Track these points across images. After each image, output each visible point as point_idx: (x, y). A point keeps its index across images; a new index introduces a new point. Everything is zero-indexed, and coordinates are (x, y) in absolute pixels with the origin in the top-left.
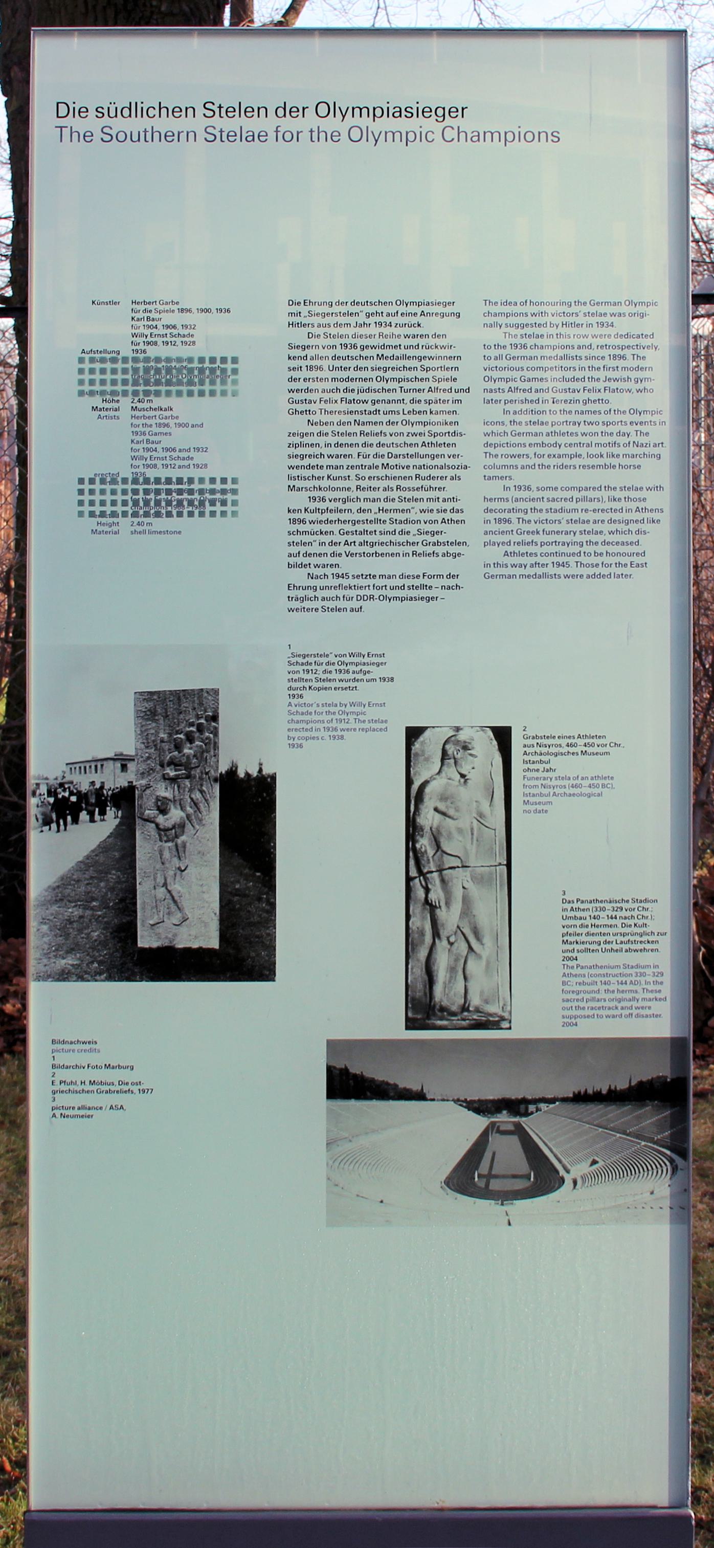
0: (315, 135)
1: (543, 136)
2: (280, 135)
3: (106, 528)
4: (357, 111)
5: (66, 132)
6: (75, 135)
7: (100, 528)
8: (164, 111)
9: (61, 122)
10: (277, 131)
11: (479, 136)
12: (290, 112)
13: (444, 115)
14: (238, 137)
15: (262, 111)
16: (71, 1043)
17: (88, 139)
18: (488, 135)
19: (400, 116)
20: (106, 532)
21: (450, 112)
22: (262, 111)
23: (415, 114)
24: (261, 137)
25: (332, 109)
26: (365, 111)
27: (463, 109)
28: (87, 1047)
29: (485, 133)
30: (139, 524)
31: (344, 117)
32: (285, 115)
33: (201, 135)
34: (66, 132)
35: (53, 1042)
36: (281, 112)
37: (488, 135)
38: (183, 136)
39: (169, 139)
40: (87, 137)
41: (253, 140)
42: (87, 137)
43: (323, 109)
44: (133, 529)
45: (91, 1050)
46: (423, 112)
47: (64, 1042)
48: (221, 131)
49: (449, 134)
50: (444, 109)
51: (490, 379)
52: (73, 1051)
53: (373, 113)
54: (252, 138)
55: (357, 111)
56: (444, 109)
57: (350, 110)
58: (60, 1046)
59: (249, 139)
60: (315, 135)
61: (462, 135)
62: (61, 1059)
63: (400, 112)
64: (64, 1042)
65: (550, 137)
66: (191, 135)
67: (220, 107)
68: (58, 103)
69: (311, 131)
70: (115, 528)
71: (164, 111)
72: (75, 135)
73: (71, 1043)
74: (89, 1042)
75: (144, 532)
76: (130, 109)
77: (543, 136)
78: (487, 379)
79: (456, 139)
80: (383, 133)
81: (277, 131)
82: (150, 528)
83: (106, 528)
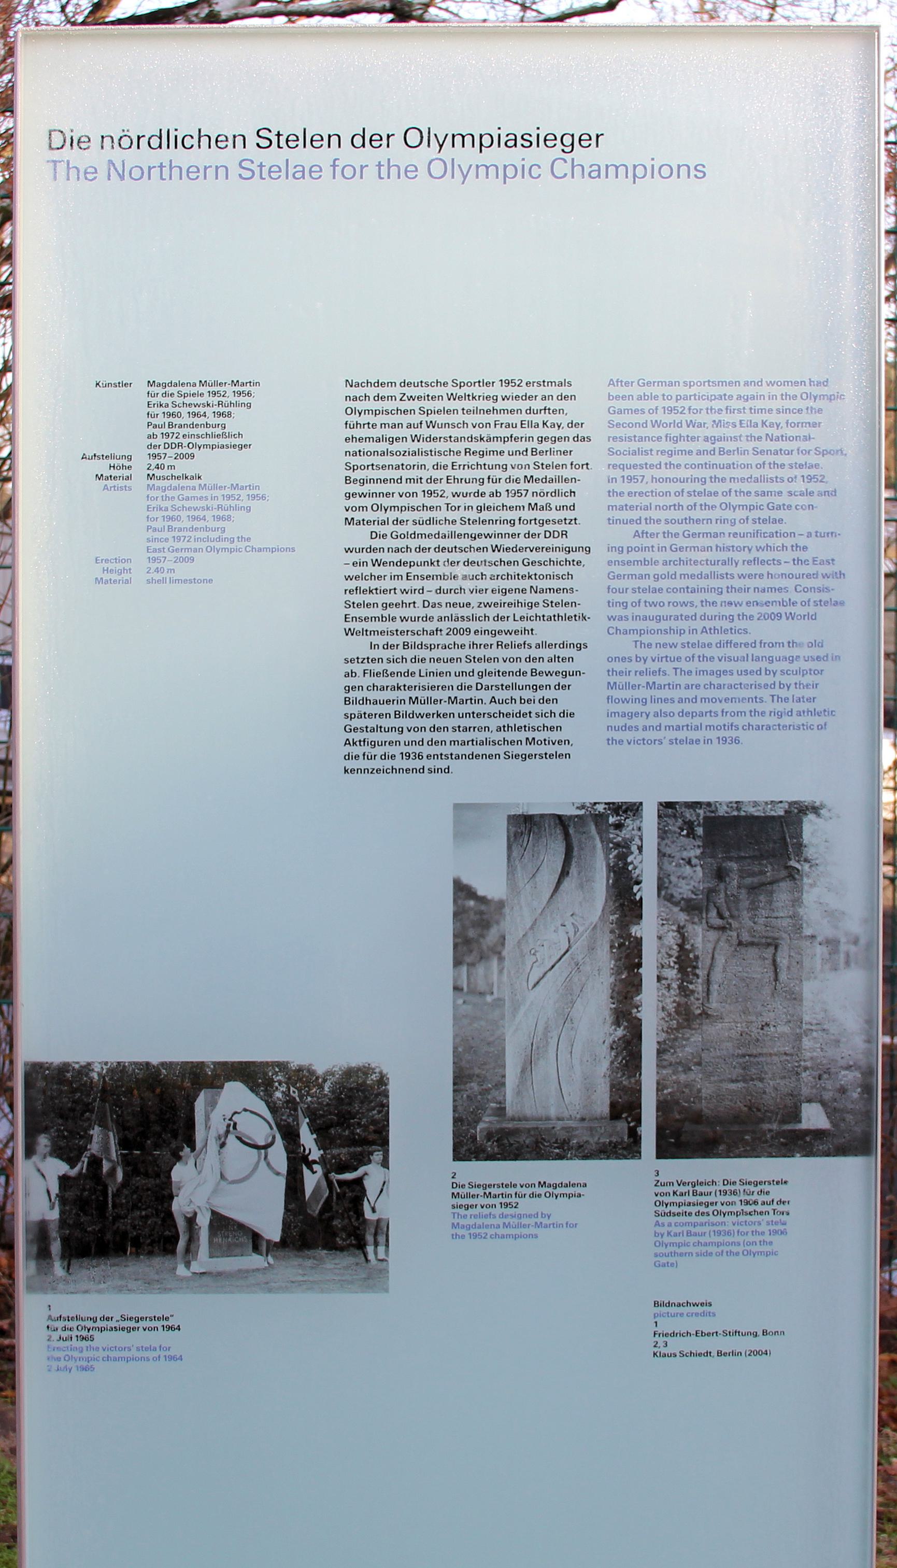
0: (384, 170)
1: (684, 170)
2: (338, 170)
3: (114, 576)
4: (458, 139)
5: (62, 168)
6: (73, 173)
7: (106, 576)
8: (205, 140)
9: (56, 155)
10: (334, 166)
11: (599, 171)
12: (371, 140)
13: (572, 144)
14: (283, 173)
15: (334, 140)
16: (679, 1305)
17: (90, 177)
18: (612, 170)
19: (515, 145)
20: (115, 581)
21: (580, 140)
22: (334, 140)
23: (535, 143)
24: (313, 172)
25: (425, 137)
26: (468, 139)
27: (598, 136)
28: (700, 1309)
29: (607, 167)
30: (157, 570)
31: (441, 146)
32: (363, 145)
33: (234, 171)
34: (62, 168)
35: (656, 1304)
36: (358, 141)
37: (612, 170)
38: (211, 172)
39: (192, 176)
40: (89, 174)
41: (303, 177)
42: (89, 174)
43: (413, 138)
44: (149, 576)
45: (704, 1314)
46: (545, 140)
47: (669, 1304)
48: (261, 166)
49: (560, 168)
50: (180, 168)
51: (353, 411)
52: (681, 1315)
53: (480, 143)
54: (302, 173)
55: (458, 139)
56: (573, 136)
57: (449, 138)
58: (664, 1310)
59: (297, 175)
60: (384, 170)
61: (578, 170)
62: (666, 1325)
63: (515, 140)
64: (669, 1304)
65: (693, 172)
66: (222, 171)
67: (279, 135)
68: (50, 132)
69: (379, 165)
70: (126, 576)
71: (205, 140)
72: (73, 173)
73: (679, 1305)
74: (702, 1304)
75: (163, 581)
76: (160, 138)
77: (684, 170)
78: (349, 411)
79: (569, 175)
80: (474, 167)
81: (334, 166)
82: (172, 575)
83: (114, 576)
